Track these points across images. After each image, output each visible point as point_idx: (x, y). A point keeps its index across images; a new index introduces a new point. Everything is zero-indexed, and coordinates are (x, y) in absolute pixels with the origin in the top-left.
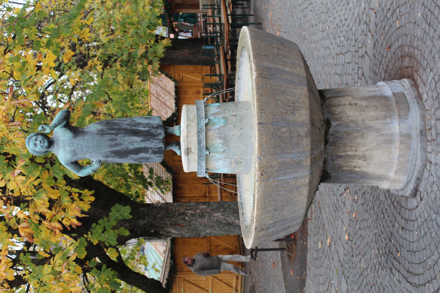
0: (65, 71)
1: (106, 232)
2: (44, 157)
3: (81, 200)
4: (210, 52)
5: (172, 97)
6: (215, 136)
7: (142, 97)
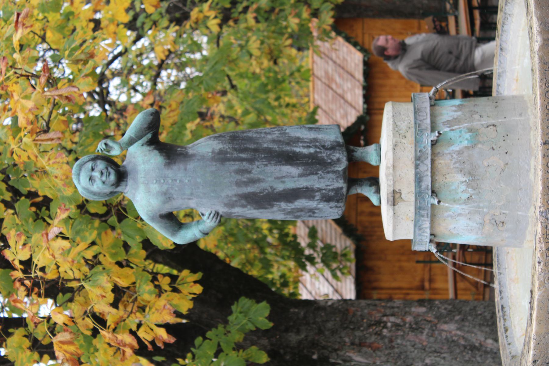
0: (146, 30)
1: (221, 355)
2: (104, 202)
3: (175, 290)
5: (357, 84)
6: (452, 167)
7: (298, 83)
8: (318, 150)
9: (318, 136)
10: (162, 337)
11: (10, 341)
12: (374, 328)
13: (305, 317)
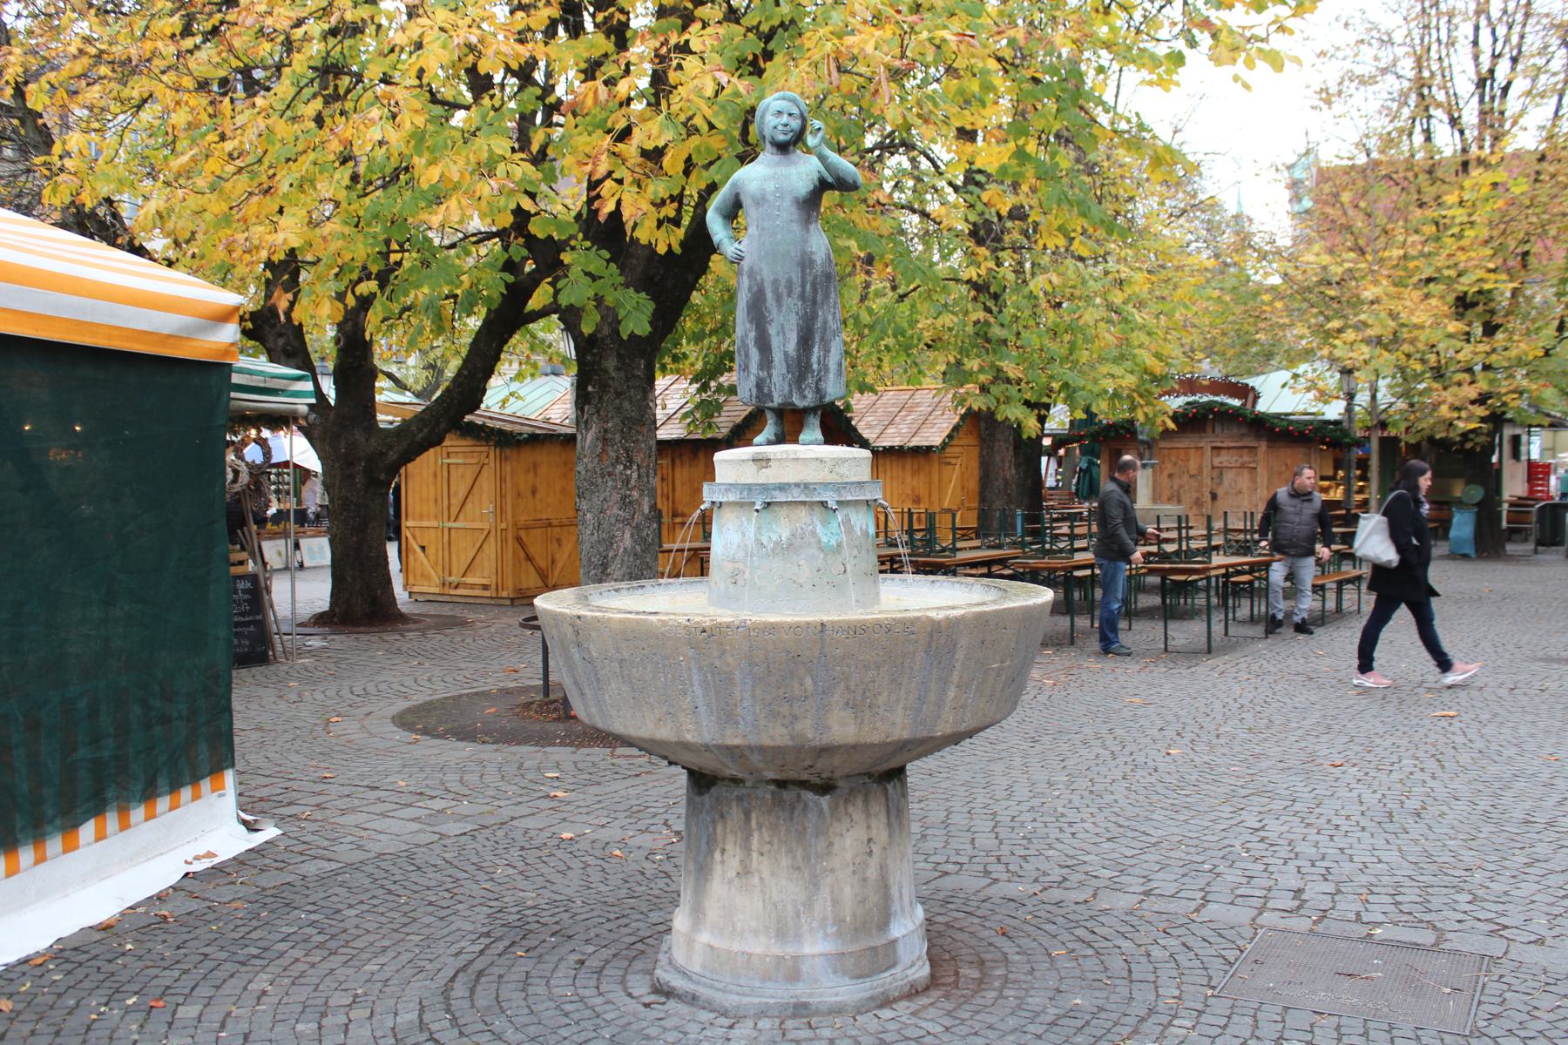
3: (660, 223)
4: (1007, 527)
11: (601, 37)
13: (635, 376)
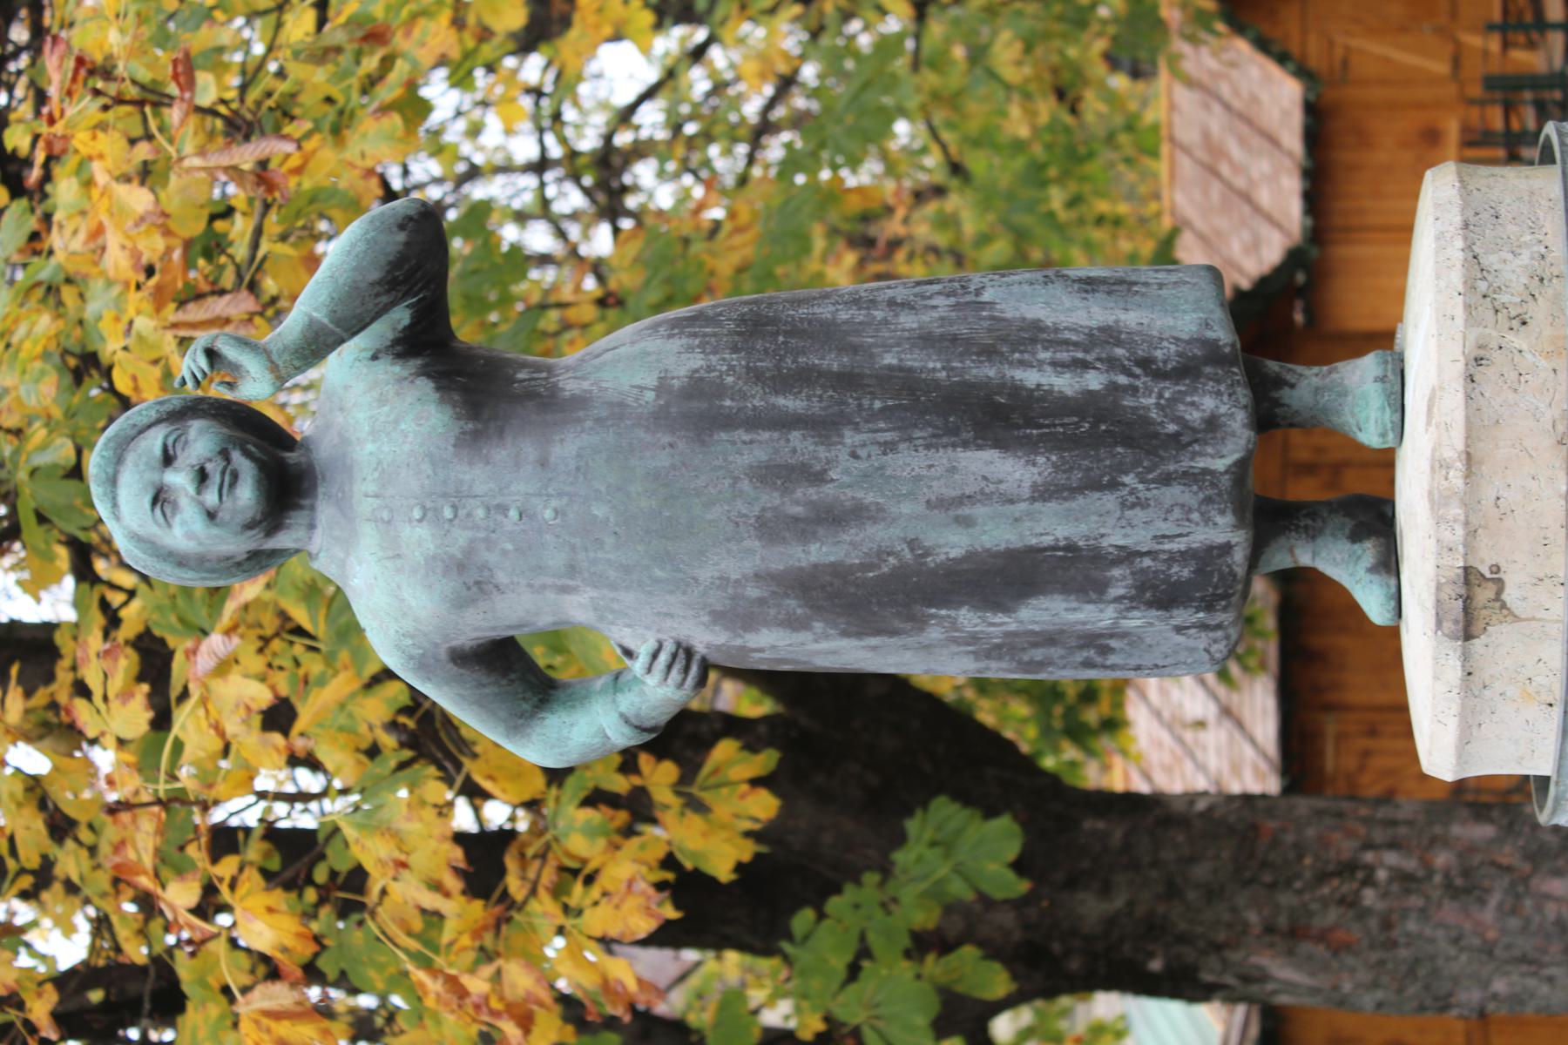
3: (696, 806)
8: (1123, 380)
9: (1123, 317)
10: (624, 987)
12: (1335, 882)
